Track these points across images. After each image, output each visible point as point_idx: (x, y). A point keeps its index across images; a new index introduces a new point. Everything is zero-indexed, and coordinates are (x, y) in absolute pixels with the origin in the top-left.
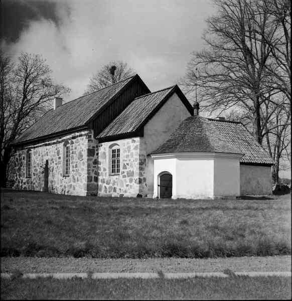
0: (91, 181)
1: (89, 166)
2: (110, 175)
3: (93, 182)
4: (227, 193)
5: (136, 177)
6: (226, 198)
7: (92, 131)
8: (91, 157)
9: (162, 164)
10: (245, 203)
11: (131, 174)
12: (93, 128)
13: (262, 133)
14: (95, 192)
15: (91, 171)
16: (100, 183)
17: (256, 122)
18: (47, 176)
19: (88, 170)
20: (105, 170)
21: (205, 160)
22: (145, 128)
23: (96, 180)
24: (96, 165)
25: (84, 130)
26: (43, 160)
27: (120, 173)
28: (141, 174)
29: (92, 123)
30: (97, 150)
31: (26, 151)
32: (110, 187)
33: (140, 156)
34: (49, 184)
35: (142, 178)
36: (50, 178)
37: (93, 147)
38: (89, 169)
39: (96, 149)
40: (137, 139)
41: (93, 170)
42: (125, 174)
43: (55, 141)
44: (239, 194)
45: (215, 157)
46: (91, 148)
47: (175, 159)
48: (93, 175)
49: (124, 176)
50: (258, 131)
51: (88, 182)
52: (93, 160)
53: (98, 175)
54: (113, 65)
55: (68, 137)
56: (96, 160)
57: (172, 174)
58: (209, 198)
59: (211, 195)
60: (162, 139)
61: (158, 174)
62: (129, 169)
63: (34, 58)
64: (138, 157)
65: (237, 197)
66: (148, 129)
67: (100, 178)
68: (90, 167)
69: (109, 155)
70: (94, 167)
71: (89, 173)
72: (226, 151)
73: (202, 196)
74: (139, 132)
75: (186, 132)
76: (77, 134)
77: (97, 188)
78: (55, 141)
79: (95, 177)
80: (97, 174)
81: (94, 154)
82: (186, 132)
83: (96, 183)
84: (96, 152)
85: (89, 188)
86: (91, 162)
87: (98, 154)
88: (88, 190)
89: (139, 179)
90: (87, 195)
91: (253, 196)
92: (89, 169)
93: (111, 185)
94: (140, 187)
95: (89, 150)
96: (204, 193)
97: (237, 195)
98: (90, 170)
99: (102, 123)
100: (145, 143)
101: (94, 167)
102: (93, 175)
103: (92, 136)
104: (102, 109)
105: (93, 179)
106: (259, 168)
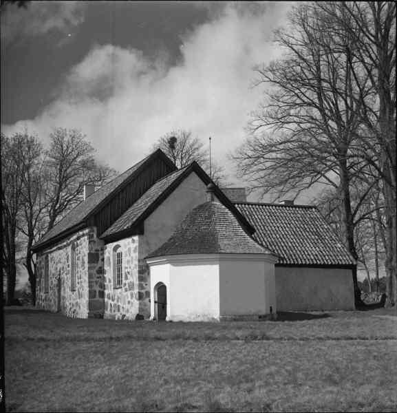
0: (95, 296)
1: (90, 276)
2: (114, 288)
3: (97, 298)
4: (242, 311)
5: (136, 291)
6: (239, 318)
7: (95, 229)
8: (93, 265)
9: (161, 272)
10: (282, 328)
11: (131, 287)
12: (96, 225)
13: (352, 219)
14: (100, 311)
15: (94, 284)
16: (106, 299)
17: (344, 204)
18: (59, 291)
19: (89, 282)
20: (110, 281)
21: (195, 262)
22: (146, 222)
23: (102, 294)
24: (101, 275)
25: (81, 229)
26: (57, 269)
27: (122, 286)
28: (141, 287)
29: (93, 218)
30: (103, 254)
31: (44, 257)
32: (115, 305)
33: (139, 261)
34: (62, 301)
35: (143, 291)
36: (62, 293)
37: (97, 250)
38: (91, 280)
39: (100, 252)
40: (136, 238)
41: (96, 282)
42: (127, 286)
43: (65, 243)
44: (263, 310)
45: (220, 260)
46: (93, 252)
47: (169, 265)
48: (97, 289)
49: (126, 291)
50: (348, 217)
51: (89, 298)
52: (97, 268)
53: (104, 289)
54: (173, 136)
55: (75, 237)
56: (100, 268)
57: (166, 285)
58: (213, 319)
59: (215, 313)
60: (165, 237)
61: (154, 285)
62: (130, 279)
63: (72, 133)
64: (137, 263)
65: (260, 317)
66: (149, 223)
67: (106, 292)
68: (92, 278)
69: (114, 261)
70: (98, 278)
71: (90, 286)
72: (247, 252)
73: (204, 316)
74: (137, 228)
75: (189, 226)
76: (81, 233)
77: (103, 306)
78: (65, 243)
79: (99, 291)
80: (103, 287)
81: (98, 260)
82: (189, 226)
83: (101, 300)
84: (101, 257)
85: (91, 306)
86: (94, 271)
87: (103, 260)
88: (90, 310)
89: (139, 292)
90: (89, 317)
91: (314, 313)
92: (91, 280)
93: (115, 301)
94: (140, 304)
95: (90, 254)
96: (206, 313)
97: (260, 314)
98: (92, 282)
99: (106, 221)
100: (148, 244)
101: (98, 278)
102: (97, 289)
103: (95, 236)
104: (106, 199)
105: (97, 293)
106: (331, 271)
